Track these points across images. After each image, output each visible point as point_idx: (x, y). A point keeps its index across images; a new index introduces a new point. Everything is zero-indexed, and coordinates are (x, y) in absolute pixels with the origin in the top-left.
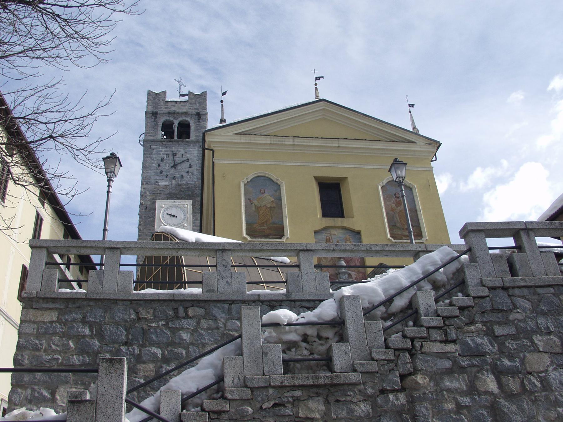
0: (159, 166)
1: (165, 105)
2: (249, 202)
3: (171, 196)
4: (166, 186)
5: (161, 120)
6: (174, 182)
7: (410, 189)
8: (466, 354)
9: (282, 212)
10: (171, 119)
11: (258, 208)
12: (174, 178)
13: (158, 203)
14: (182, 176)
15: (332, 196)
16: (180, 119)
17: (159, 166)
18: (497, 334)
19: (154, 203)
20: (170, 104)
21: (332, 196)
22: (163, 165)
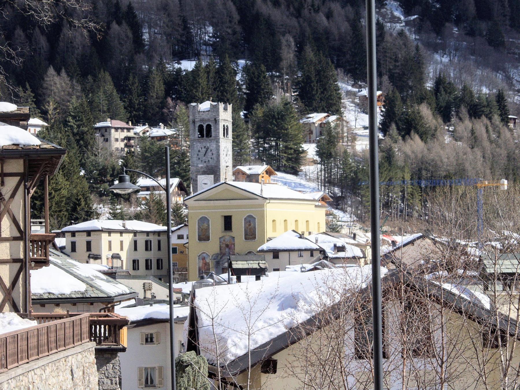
0: (198, 155)
1: (199, 114)
2: (199, 226)
3: (205, 173)
4: (202, 167)
5: (197, 125)
6: (205, 164)
7: (120, 304)
8: (383, 271)
9: (225, 221)
10: (202, 124)
11: (202, 229)
12: (205, 162)
13: (199, 176)
14: (209, 161)
15: (228, 222)
16: (207, 124)
17: (198, 155)
18: (134, 300)
19: (197, 177)
20: (201, 113)
21: (228, 222)
22: (200, 153)
